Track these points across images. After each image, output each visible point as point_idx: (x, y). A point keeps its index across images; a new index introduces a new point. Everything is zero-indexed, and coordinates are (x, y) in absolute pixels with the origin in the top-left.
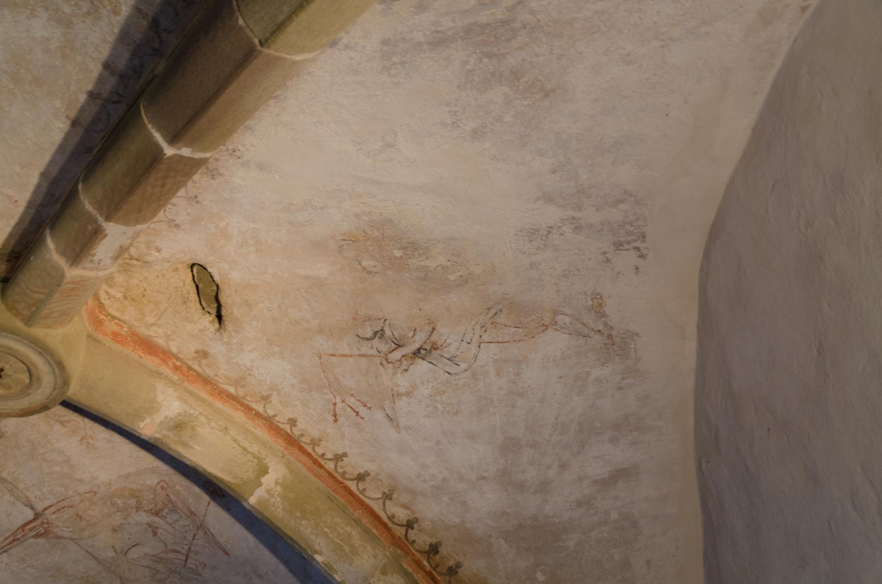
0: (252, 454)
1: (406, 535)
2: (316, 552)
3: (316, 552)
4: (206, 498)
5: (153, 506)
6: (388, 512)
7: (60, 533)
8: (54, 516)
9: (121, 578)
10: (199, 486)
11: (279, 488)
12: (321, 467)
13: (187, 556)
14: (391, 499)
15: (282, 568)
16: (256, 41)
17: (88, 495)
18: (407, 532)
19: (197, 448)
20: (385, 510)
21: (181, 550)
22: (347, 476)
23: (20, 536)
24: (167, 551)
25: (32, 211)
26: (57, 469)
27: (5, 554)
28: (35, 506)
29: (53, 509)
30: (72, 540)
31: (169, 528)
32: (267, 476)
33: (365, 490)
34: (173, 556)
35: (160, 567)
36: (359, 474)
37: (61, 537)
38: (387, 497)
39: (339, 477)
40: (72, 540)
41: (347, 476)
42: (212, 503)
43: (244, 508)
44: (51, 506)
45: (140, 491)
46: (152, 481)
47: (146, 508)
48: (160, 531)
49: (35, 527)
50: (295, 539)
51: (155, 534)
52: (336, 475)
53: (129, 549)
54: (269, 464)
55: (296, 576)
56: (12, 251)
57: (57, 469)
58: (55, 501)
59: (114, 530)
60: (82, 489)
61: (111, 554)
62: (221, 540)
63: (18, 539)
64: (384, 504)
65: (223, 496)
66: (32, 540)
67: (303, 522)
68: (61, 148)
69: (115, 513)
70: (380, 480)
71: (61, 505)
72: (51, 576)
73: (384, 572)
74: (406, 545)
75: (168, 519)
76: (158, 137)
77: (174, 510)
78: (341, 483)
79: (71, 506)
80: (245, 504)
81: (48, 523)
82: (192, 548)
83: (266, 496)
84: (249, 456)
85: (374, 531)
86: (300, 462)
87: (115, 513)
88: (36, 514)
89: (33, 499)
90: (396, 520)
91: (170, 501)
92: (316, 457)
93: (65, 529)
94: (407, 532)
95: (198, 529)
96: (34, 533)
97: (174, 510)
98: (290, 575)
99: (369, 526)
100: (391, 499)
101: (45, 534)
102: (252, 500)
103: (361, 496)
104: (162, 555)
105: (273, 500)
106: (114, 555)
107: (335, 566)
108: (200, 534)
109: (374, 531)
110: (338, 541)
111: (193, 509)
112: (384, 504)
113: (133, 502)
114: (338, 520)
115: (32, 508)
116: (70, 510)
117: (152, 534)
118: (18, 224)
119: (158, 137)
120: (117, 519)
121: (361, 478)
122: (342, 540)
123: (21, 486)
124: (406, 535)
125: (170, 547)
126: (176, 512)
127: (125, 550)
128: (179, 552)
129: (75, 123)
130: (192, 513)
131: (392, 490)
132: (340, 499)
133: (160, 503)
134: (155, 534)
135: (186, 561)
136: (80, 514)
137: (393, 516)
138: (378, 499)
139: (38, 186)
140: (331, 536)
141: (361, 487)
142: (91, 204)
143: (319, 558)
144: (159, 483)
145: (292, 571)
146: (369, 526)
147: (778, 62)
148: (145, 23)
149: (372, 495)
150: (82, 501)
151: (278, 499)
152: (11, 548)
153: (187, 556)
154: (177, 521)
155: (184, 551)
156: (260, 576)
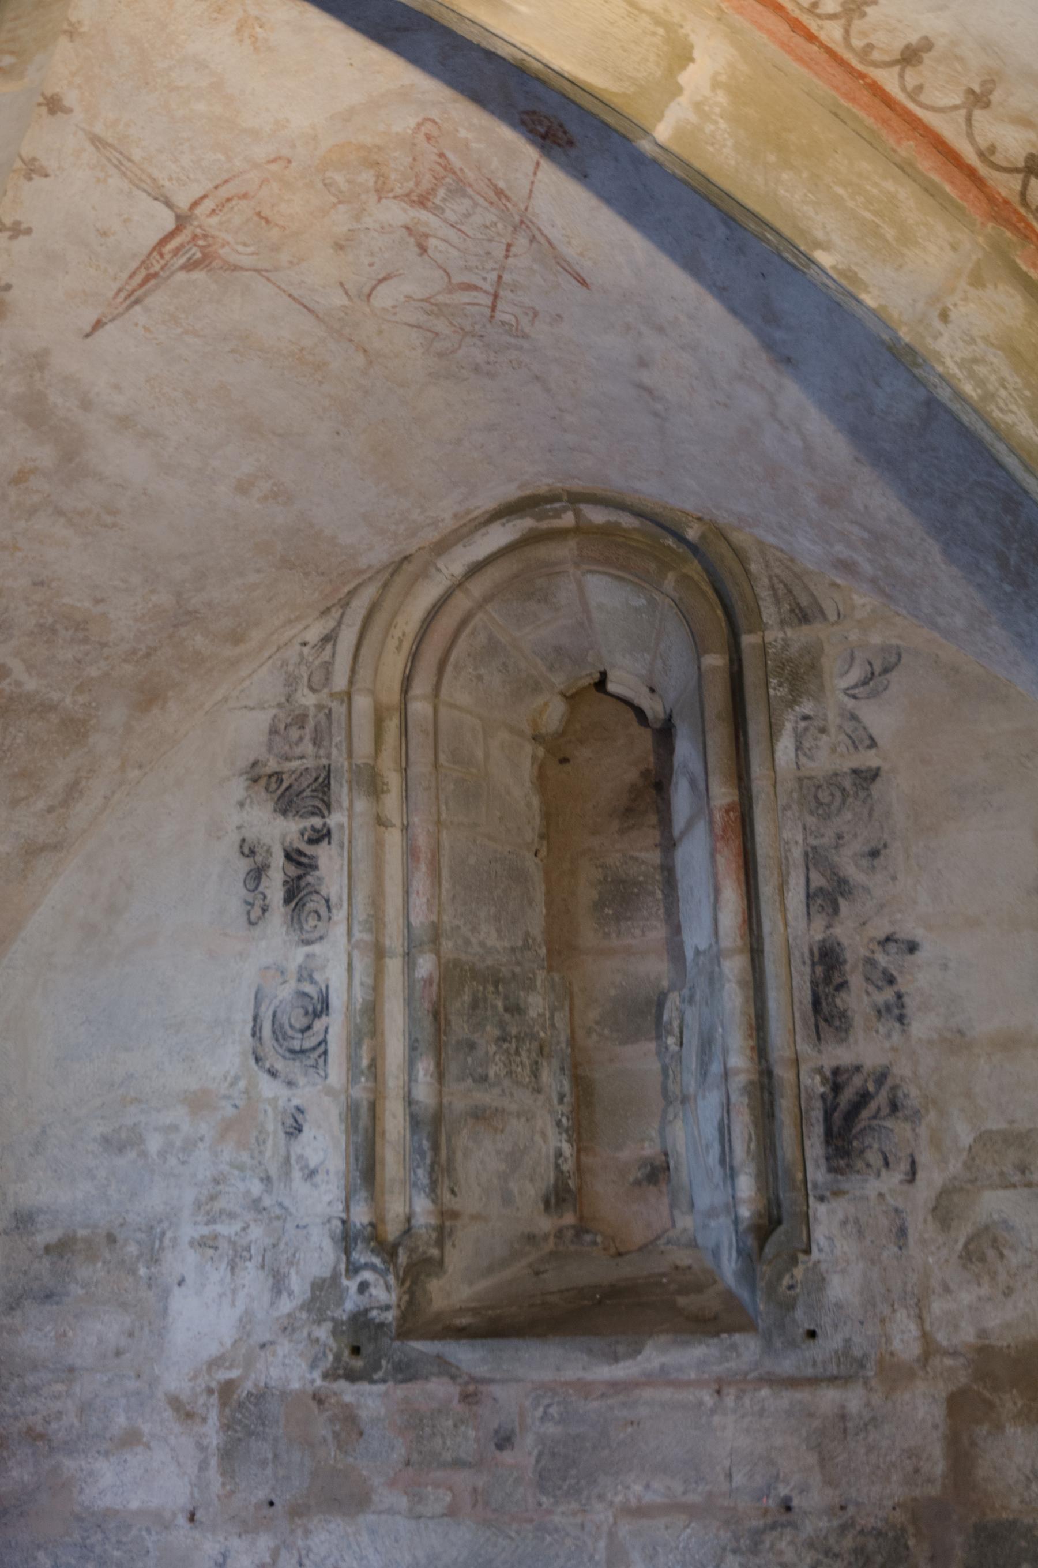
0: (651, 14)
1: (1023, 194)
2: (818, 245)
3: (818, 245)
4: (530, 152)
5: (411, 184)
6: (979, 140)
7: (233, 258)
8: (214, 221)
9: (365, 351)
10: (513, 125)
11: (721, 98)
12: (811, 38)
13: (496, 296)
14: (987, 105)
15: (713, 306)
17: (273, 167)
18: (1025, 186)
19: (523, 9)
20: (970, 136)
21: (480, 283)
22: (876, 56)
23: (157, 267)
24: (451, 289)
26: (201, 107)
27: (138, 308)
28: (174, 199)
29: (208, 204)
30: (258, 271)
31: (452, 234)
32: (691, 67)
33: (920, 88)
34: (465, 297)
35: (441, 325)
36: (908, 47)
37: (236, 268)
38: (978, 100)
39: (854, 62)
40: (258, 271)
41: (876, 56)
42: (546, 165)
43: (639, 159)
44: (205, 197)
45: (380, 148)
46: (404, 122)
47: (399, 191)
48: (432, 242)
49: (182, 246)
50: (767, 215)
51: (423, 250)
52: (847, 56)
53: (374, 288)
54: (693, 38)
55: (745, 320)
57: (201, 107)
58: (210, 186)
59: (339, 247)
60: (261, 152)
61: (339, 300)
62: (570, 252)
63: (155, 275)
64: (969, 119)
65: (571, 143)
66: (182, 276)
67: (785, 176)
69: (334, 205)
70: (960, 59)
71: (224, 192)
72: (232, 351)
73: (977, 280)
74: (1022, 219)
75: (449, 215)
77: (460, 189)
78: (862, 76)
79: (245, 196)
80: (645, 146)
81: (205, 236)
82: (507, 277)
83: (693, 118)
84: (645, 21)
85: (948, 188)
86: (761, 27)
87: (334, 205)
88: (178, 217)
89: (167, 184)
90: (999, 159)
91: (448, 168)
92: (797, 13)
93: (240, 248)
94: (1025, 186)
95: (515, 229)
96: (182, 261)
97: (460, 189)
98: (729, 319)
99: (936, 178)
100: (987, 105)
101: (203, 262)
102: (663, 132)
103: (912, 106)
104: (441, 298)
105: (709, 128)
106: (345, 301)
107: (862, 275)
108: (522, 242)
109: (948, 188)
110: (868, 215)
111: (501, 184)
112: (969, 119)
113: (367, 177)
114: (865, 166)
115: (168, 204)
116: (243, 203)
117: (416, 250)
120: (340, 221)
121: (910, 57)
122: (876, 213)
123: (137, 154)
124: (1023, 194)
125: (457, 279)
126: (465, 195)
127: (366, 290)
128: (476, 288)
130: (499, 193)
131: (990, 83)
132: (862, 114)
133: (428, 176)
134: (423, 250)
135: (493, 308)
136: (267, 212)
137: (993, 149)
138: (956, 108)
140: (850, 204)
141: (911, 81)
143: (823, 257)
144: (419, 125)
145: (733, 311)
146: (936, 178)
149: (938, 98)
150: (264, 182)
151: (723, 125)
152: (146, 295)
153: (496, 296)
154: (467, 215)
155: (487, 286)
156: (660, 329)
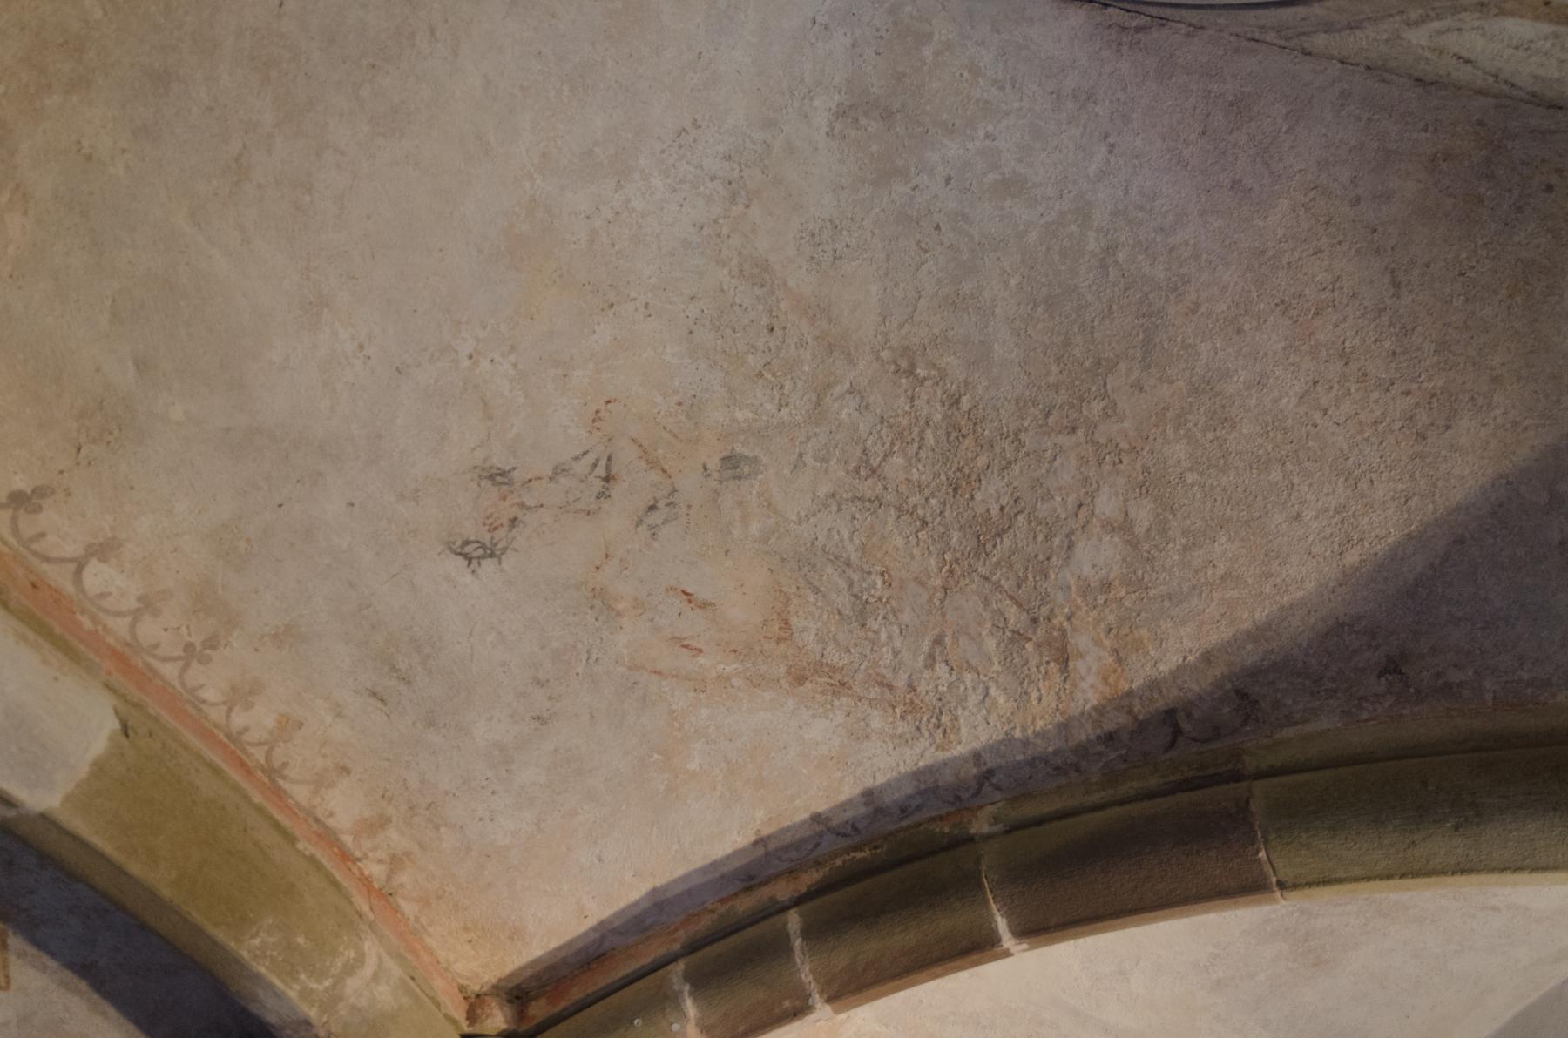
16: (1274, 880)
25: (597, 935)
56: (518, 987)
68: (714, 865)
76: (1002, 924)
118: (559, 949)
119: (1002, 924)
129: (760, 842)
139: (636, 904)
142: (813, 972)
147: (1535, 996)
148: (975, 771)
